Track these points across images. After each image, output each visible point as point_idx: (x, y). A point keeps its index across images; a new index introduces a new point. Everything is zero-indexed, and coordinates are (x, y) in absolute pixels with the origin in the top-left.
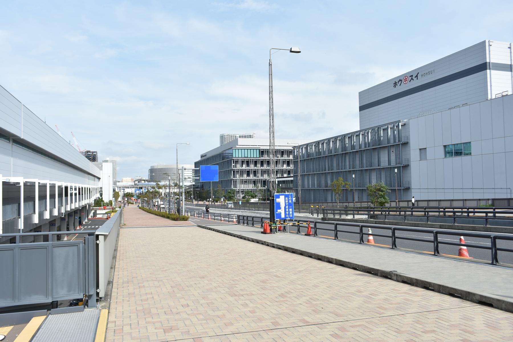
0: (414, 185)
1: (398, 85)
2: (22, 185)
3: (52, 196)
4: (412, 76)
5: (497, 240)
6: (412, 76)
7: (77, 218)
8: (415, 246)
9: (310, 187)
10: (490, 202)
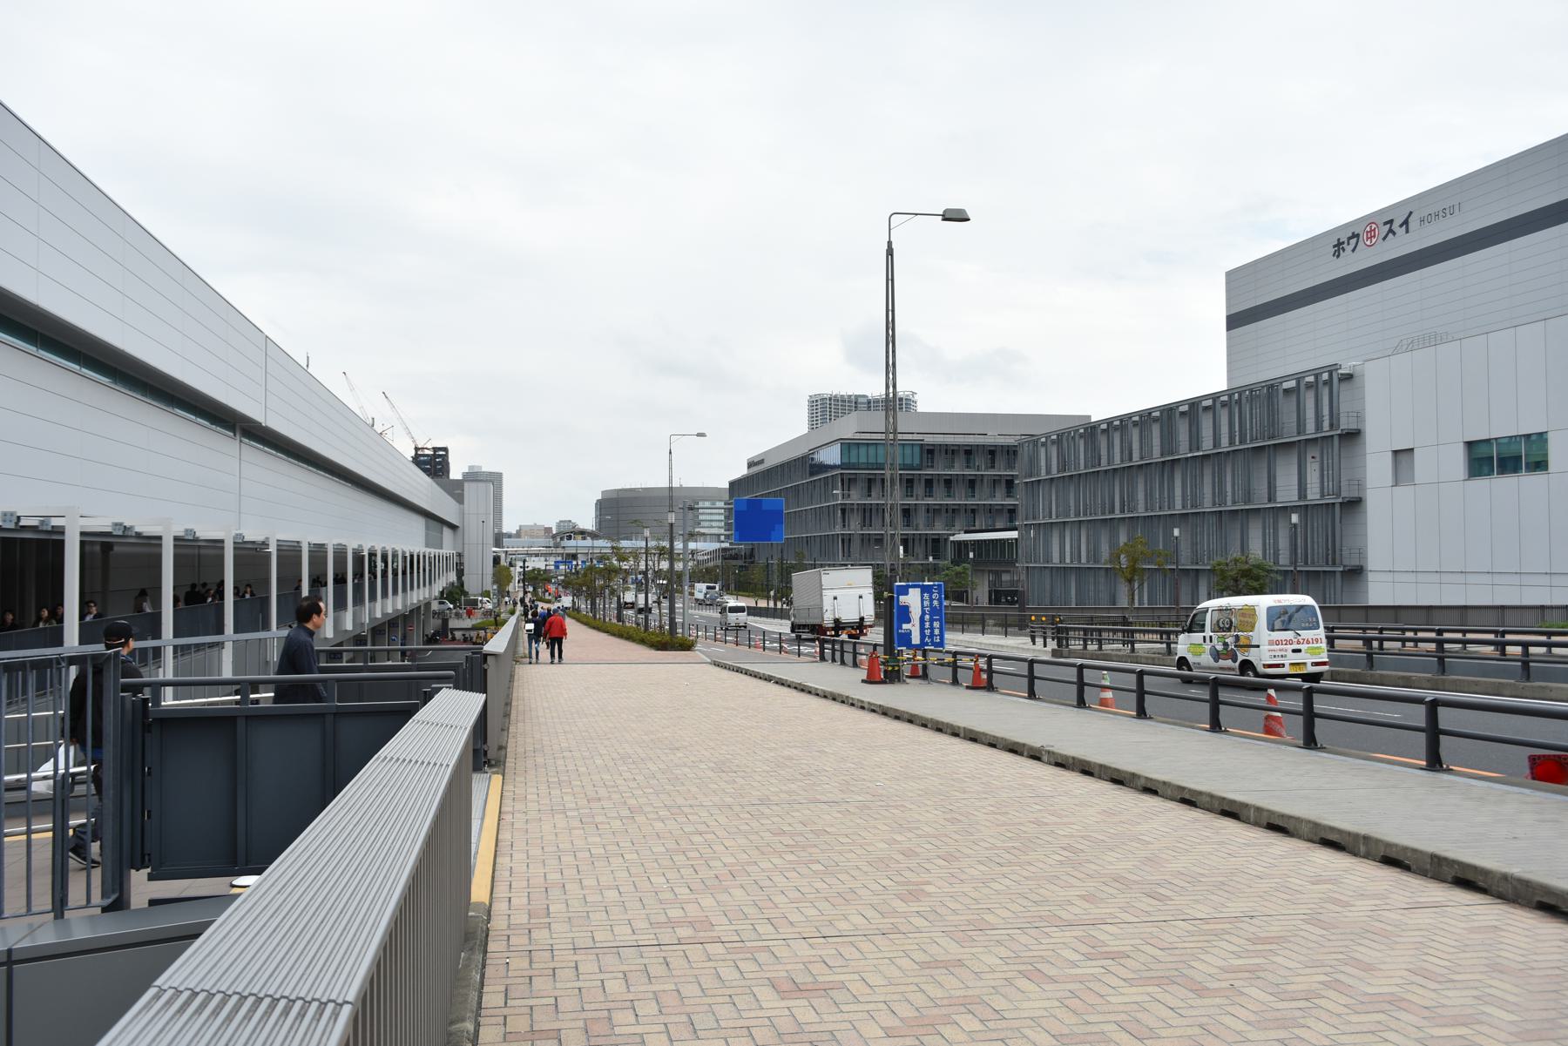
1: (1349, 248)
2: (273, 549)
3: (340, 580)
4: (1391, 222)
5: (1441, 710)
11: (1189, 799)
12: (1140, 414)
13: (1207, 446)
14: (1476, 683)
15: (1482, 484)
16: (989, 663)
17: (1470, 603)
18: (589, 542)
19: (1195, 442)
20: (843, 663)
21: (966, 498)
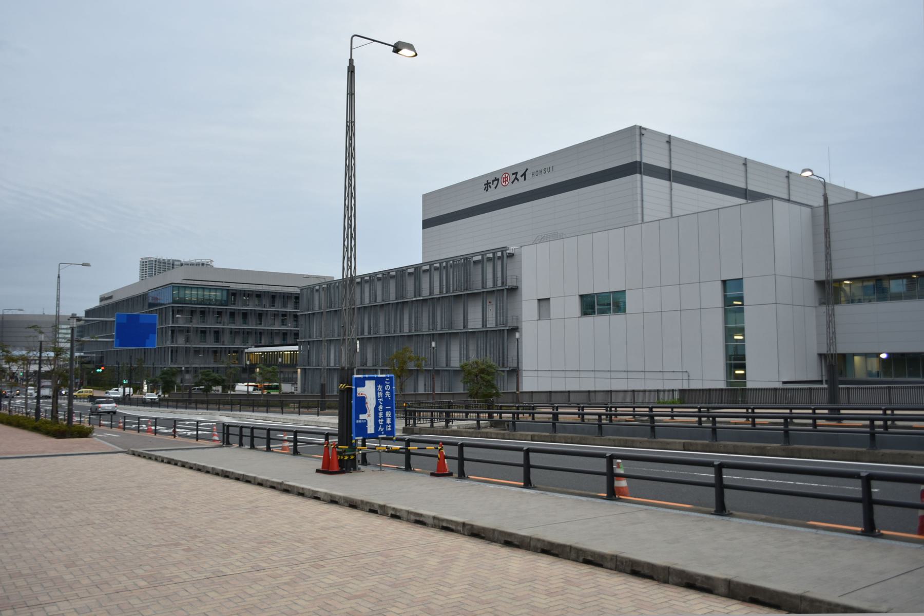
0: (528, 362)
1: (493, 186)
4: (516, 173)
6: (517, 173)
8: (568, 480)
9: (332, 364)
12: (382, 273)
13: (425, 293)
14: (834, 452)
15: (589, 319)
16: (252, 432)
17: (553, 390)
19: (418, 291)
21: (257, 325)
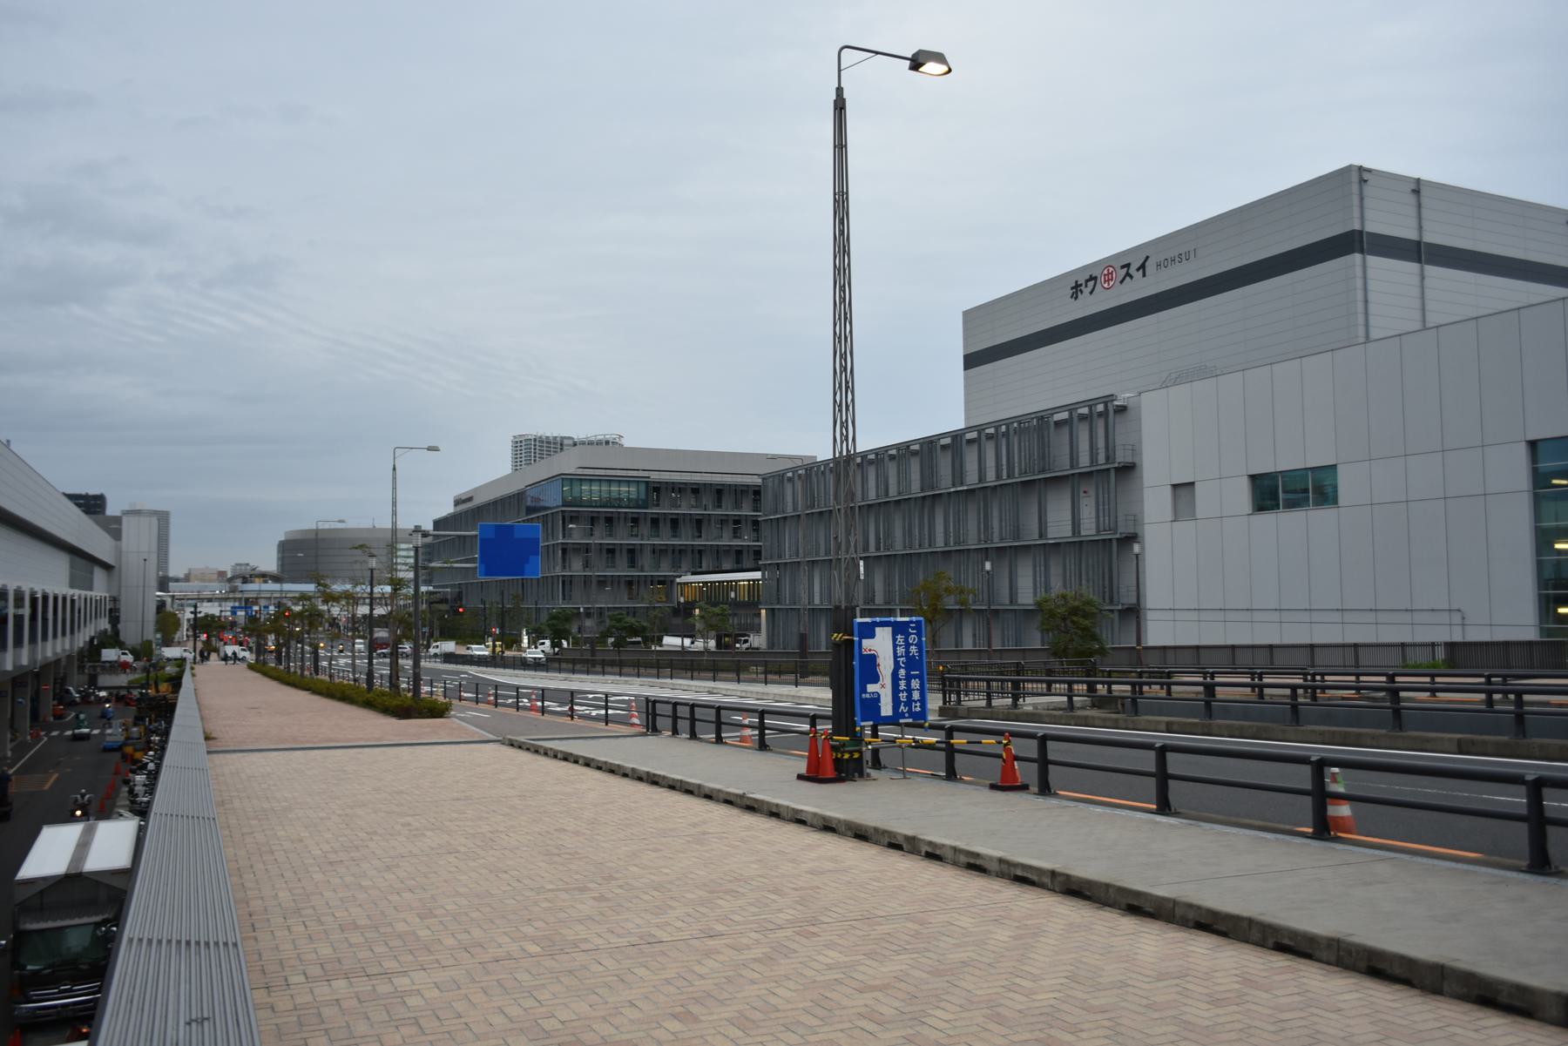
0: (1155, 596)
1: (1087, 291)
4: (1128, 266)
5: (1170, 756)
6: (1129, 265)
7: (25, 702)
9: (817, 601)
10: (1441, 654)
11: (975, 865)
12: (897, 446)
13: (972, 479)
15: (1268, 518)
18: (271, 586)
20: (693, 736)
21: (693, 538)
